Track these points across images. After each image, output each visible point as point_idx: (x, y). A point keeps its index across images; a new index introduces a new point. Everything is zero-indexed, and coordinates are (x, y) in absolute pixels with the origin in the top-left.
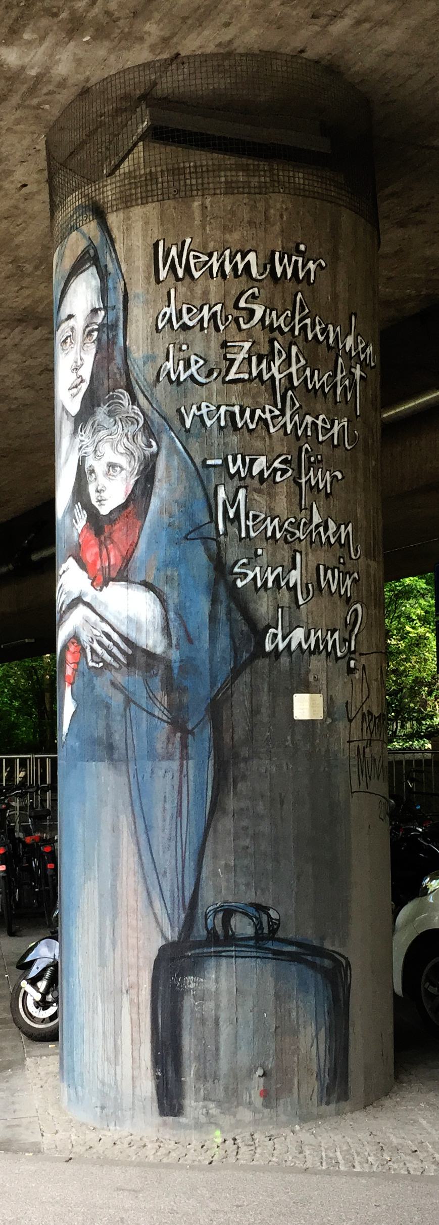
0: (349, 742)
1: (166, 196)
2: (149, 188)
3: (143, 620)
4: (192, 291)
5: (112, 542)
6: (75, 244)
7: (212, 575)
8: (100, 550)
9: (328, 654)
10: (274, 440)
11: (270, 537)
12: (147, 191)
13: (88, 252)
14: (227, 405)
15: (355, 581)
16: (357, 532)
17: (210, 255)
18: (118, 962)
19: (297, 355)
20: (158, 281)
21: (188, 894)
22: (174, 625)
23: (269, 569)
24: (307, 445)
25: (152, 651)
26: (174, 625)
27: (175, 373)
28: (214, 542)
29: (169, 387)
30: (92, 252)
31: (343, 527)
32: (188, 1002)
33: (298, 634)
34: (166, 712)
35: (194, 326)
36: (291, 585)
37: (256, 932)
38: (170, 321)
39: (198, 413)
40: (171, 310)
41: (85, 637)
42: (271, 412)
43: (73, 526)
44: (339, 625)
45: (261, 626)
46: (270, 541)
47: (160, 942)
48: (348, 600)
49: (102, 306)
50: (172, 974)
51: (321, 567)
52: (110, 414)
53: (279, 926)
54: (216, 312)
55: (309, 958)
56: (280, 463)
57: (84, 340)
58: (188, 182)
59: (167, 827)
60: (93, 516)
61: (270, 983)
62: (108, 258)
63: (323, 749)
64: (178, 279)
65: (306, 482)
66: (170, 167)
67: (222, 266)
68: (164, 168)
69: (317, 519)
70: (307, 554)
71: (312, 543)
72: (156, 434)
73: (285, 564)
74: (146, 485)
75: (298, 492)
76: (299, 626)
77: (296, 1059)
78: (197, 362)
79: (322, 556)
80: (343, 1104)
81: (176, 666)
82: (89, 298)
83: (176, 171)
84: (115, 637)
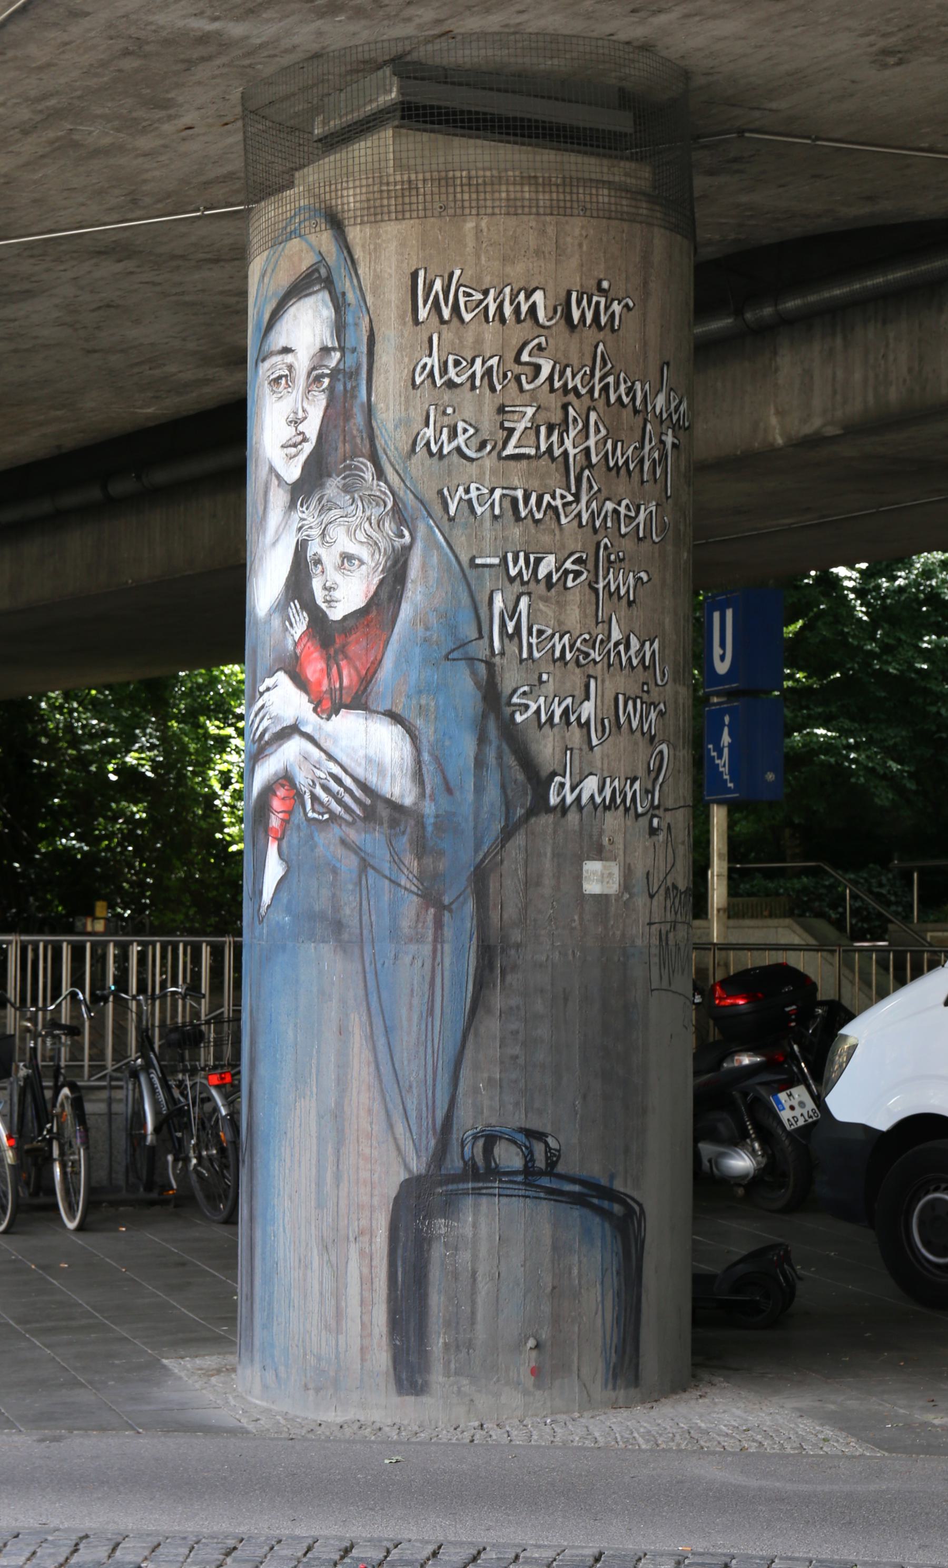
0: (650, 924)
1: (429, 213)
2: (407, 200)
3: (387, 760)
4: (461, 339)
5: (346, 657)
6: (298, 255)
7: (480, 706)
8: (328, 665)
9: (627, 810)
10: (567, 532)
11: (559, 659)
12: (403, 204)
13: (317, 270)
14: (503, 488)
15: (661, 714)
16: (664, 648)
17: (486, 293)
18: (343, 1203)
19: (596, 423)
20: (416, 322)
21: (440, 1115)
22: (429, 769)
23: (557, 699)
24: (606, 540)
25: (399, 801)
26: (429, 769)
27: (436, 443)
28: (483, 665)
29: (428, 461)
30: (323, 271)
31: (647, 644)
32: (437, 1252)
33: (590, 785)
34: (415, 881)
35: (462, 384)
36: (583, 721)
37: (526, 1165)
38: (431, 374)
39: (466, 497)
40: (433, 362)
41: (302, 779)
42: (563, 497)
43: (287, 629)
44: (641, 772)
45: (544, 773)
46: (558, 664)
47: (403, 1176)
48: (652, 738)
49: (336, 345)
50: (417, 1216)
51: (621, 697)
52: (346, 489)
53: (559, 1157)
54: (492, 366)
55: (595, 1201)
56: (573, 563)
57: (308, 386)
58: (459, 196)
59: (415, 1028)
60: (318, 619)
61: (546, 1231)
62: (348, 284)
63: (618, 933)
64: (442, 322)
65: (604, 588)
66: (435, 175)
67: (500, 308)
68: (428, 175)
69: (616, 635)
70: (603, 681)
71: (609, 665)
72: (409, 520)
73: (576, 693)
74: (394, 588)
75: (594, 600)
76: (591, 774)
77: (576, 1329)
78: (465, 431)
79: (620, 683)
80: (632, 1391)
81: (430, 821)
82: (318, 332)
83: (444, 181)
84: (348, 781)
